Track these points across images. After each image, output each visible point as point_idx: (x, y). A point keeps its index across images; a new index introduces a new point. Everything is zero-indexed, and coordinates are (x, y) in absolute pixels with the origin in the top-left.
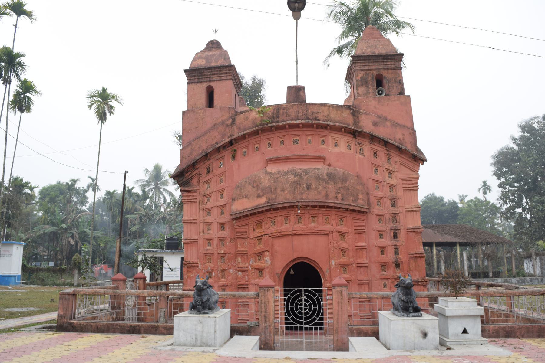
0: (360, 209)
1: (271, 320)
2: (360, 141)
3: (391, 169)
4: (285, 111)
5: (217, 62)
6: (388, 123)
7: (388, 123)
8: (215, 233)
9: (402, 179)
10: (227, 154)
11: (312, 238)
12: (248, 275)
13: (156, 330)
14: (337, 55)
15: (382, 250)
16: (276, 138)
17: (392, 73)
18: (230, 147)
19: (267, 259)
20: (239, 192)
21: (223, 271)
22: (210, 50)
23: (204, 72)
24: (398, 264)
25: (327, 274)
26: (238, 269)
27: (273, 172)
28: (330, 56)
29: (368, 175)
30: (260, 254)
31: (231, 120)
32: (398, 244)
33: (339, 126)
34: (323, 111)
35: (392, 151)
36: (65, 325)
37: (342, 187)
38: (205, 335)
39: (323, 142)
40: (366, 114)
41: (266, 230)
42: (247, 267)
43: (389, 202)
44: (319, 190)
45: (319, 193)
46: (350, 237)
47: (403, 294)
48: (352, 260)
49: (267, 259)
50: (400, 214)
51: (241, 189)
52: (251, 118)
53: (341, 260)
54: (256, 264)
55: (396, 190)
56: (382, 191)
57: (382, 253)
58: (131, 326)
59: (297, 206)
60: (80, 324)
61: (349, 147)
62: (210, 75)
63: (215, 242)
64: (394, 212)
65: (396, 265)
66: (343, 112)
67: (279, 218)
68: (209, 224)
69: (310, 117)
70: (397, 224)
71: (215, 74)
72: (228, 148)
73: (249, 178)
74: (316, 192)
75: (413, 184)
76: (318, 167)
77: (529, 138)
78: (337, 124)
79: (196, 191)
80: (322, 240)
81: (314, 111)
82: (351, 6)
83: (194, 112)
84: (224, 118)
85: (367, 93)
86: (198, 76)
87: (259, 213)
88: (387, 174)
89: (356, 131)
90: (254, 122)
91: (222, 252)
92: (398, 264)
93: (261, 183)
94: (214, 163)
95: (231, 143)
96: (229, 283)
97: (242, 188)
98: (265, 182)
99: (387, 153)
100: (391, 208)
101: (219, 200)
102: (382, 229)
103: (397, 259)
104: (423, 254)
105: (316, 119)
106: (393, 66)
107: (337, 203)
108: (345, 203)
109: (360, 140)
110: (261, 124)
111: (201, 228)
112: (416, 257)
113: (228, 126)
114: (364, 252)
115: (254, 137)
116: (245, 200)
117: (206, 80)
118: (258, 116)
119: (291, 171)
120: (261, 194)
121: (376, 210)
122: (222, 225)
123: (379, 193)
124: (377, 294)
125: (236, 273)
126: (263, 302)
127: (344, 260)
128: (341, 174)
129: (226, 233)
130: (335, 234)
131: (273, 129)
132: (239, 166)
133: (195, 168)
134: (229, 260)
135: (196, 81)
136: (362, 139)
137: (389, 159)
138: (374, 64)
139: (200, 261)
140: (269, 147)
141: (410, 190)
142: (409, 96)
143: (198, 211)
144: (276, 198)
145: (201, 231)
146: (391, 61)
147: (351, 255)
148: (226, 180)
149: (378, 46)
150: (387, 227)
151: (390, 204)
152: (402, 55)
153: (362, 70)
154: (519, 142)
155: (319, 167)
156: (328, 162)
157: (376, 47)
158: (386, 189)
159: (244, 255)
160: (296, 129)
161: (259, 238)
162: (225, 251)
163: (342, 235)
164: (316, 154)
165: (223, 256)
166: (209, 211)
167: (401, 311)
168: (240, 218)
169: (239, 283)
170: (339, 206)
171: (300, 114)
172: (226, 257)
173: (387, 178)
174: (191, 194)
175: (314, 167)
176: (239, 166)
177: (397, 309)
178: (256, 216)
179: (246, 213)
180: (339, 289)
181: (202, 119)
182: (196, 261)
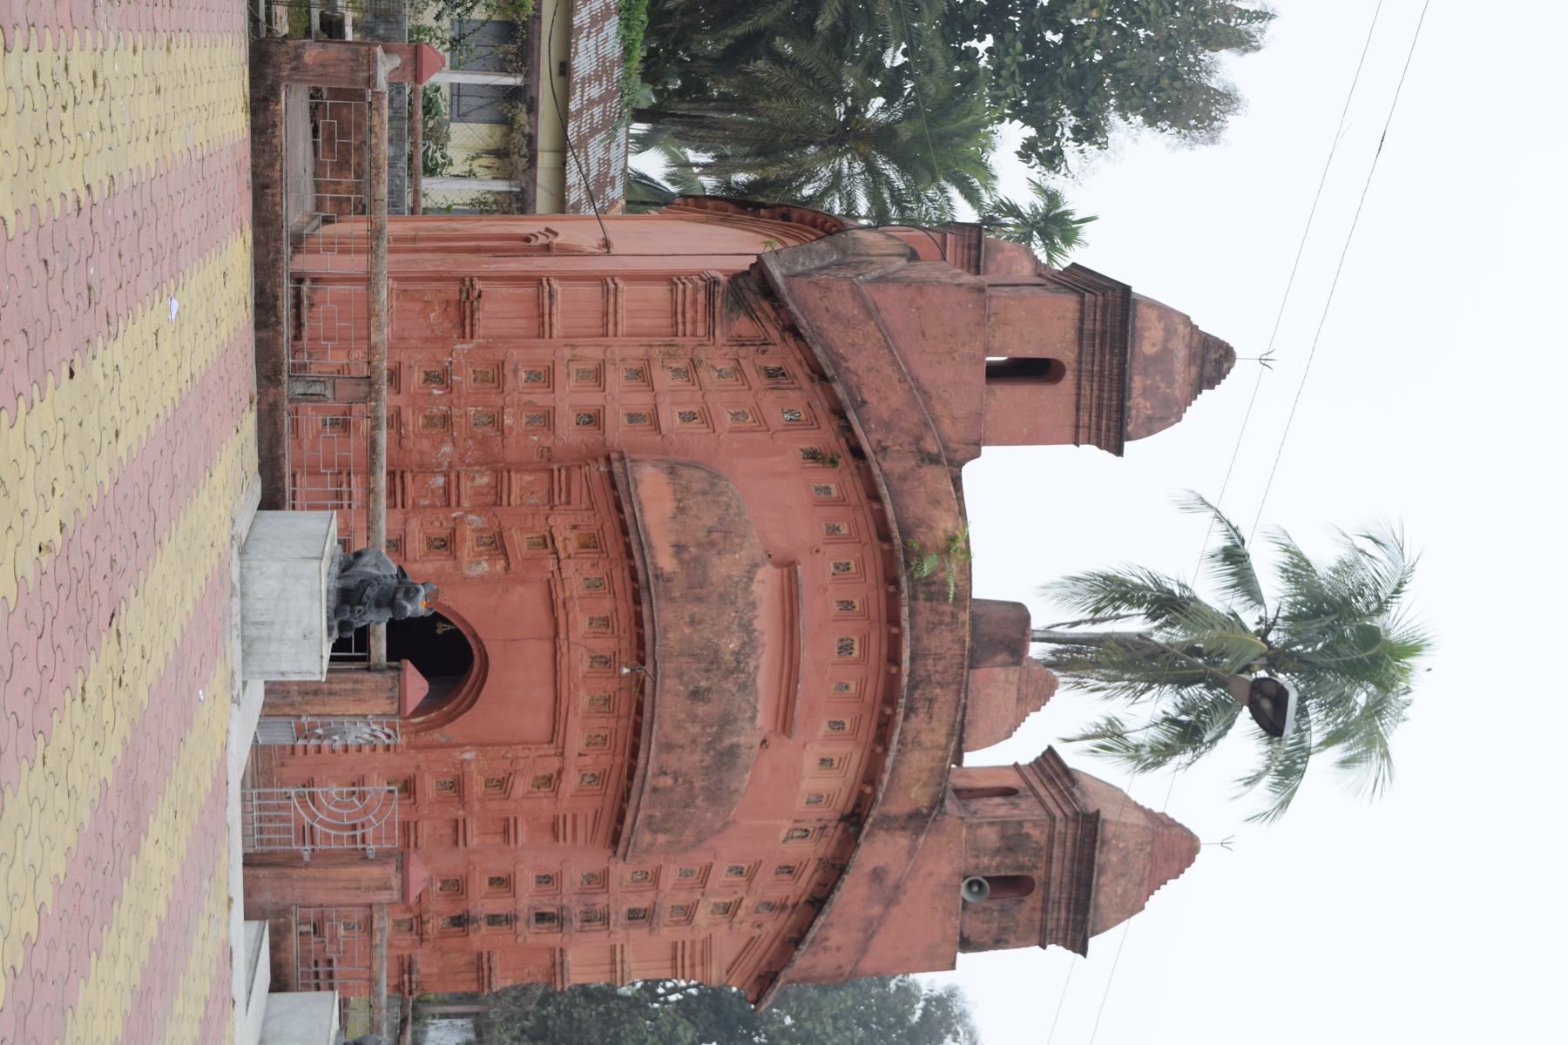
0: (624, 836)
1: (309, 708)
2: (830, 830)
3: (741, 913)
4: (947, 619)
5: (1143, 395)
6: (877, 910)
7: (877, 910)
8: (569, 398)
9: (708, 943)
10: (825, 436)
11: (543, 694)
12: (433, 506)
13: (268, 378)
14: (1220, 541)
15: (502, 883)
16: (865, 591)
17: (1031, 920)
18: (845, 448)
19: (485, 566)
20: (696, 487)
21: (446, 420)
23: (1112, 354)
24: (461, 922)
26: (453, 476)
27: (754, 587)
28: (1220, 518)
30: (497, 545)
31: (935, 450)
32: (520, 925)
33: (881, 781)
35: (794, 916)
36: (269, 71)
37: (692, 788)
38: (273, 648)
39: (837, 725)
40: (911, 852)
41: (572, 562)
42: (458, 504)
44: (688, 725)
46: (544, 805)
48: (476, 806)
49: (485, 566)
51: (704, 493)
52: (937, 513)
53: (476, 775)
55: (677, 923)
56: (676, 887)
57: (492, 881)
58: (276, 298)
60: (274, 125)
61: (817, 800)
62: (1102, 376)
63: (540, 398)
64: (613, 917)
66: (925, 785)
68: (598, 376)
69: (917, 694)
70: (577, 924)
71: (1101, 390)
72: (842, 441)
73: (740, 514)
74: (683, 716)
75: (693, 966)
77: (902, 1019)
78: (886, 778)
79: (710, 332)
80: (536, 724)
81: (936, 706)
83: (979, 324)
84: (946, 426)
85: (977, 851)
86: (1104, 333)
87: (628, 547)
88: (727, 900)
89: (860, 826)
90: (920, 523)
91: (508, 421)
94: (799, 397)
95: (857, 452)
97: (710, 498)
98: (722, 568)
99: (790, 903)
100: (624, 909)
101: (677, 410)
102: (566, 885)
103: (476, 920)
104: (490, 987)
105: (911, 710)
106: (1051, 925)
108: (645, 798)
109: (834, 833)
112: (479, 968)
113: (918, 439)
114: (499, 839)
115: (871, 522)
116: (669, 507)
117: (1086, 358)
119: (752, 640)
120: (686, 556)
121: (621, 872)
122: (593, 419)
123: (670, 876)
125: (440, 465)
126: (358, 686)
127: (476, 787)
128: (734, 785)
129: (568, 432)
131: (892, 589)
132: (784, 475)
133: (786, 335)
134: (483, 442)
135: (1088, 325)
137: (771, 907)
138: (1067, 874)
139: (479, 346)
140: (837, 567)
141: (674, 958)
143: (645, 340)
144: (672, 599)
145: (578, 351)
146: (1067, 920)
149: (1123, 882)
151: (636, 906)
153: (1051, 838)
155: (759, 721)
156: (773, 740)
157: (1123, 875)
158: (683, 898)
159: (496, 498)
160: (884, 651)
162: (511, 428)
163: (551, 782)
165: (496, 421)
166: (641, 375)
168: (614, 486)
169: (408, 477)
170: (637, 780)
171: (930, 662)
172: (489, 431)
173: (713, 900)
174: (700, 316)
175: (760, 706)
176: (784, 475)
178: (619, 534)
179: (627, 509)
180: (395, 882)
182: (479, 331)
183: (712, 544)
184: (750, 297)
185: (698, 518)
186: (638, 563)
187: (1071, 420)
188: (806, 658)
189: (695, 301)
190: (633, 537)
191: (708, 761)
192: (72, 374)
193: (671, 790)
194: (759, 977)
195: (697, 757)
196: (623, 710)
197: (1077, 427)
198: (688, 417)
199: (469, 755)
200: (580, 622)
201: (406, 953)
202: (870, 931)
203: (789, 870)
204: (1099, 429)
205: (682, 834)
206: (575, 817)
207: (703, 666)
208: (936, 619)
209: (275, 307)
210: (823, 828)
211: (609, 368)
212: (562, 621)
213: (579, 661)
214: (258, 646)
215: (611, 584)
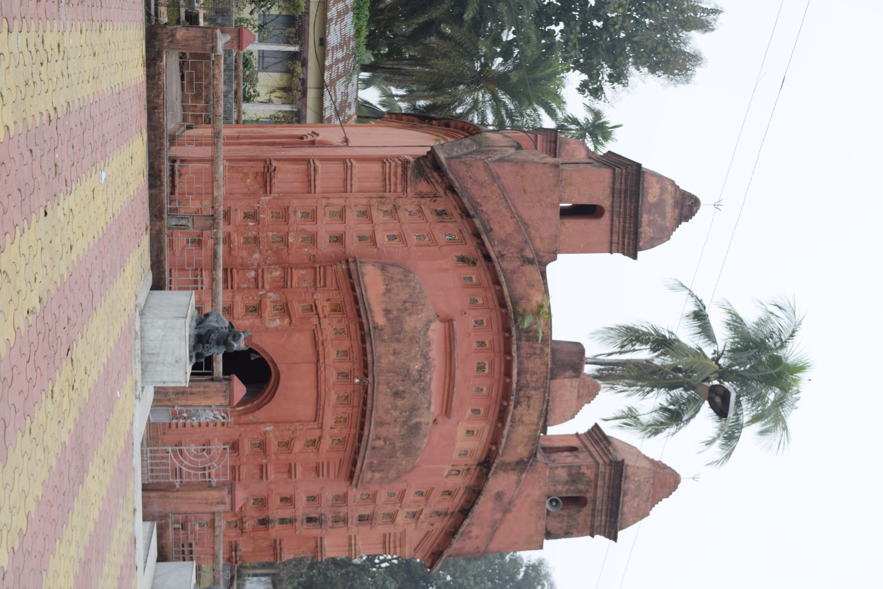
0: (356, 474)
1: (179, 402)
2: (472, 471)
3: (422, 517)
4: (538, 352)
5: (648, 225)
6: (498, 516)
7: (498, 516)
8: (325, 227)
9: (403, 534)
10: (469, 249)
11: (311, 394)
12: (249, 288)
13: (156, 216)
15: (288, 500)
16: (491, 336)
17: (585, 522)
18: (480, 255)
19: (278, 322)
20: (397, 277)
21: (256, 239)
23: (631, 202)
24: (264, 522)
25: (251, 417)
26: (260, 271)
27: (429, 333)
29: (414, 483)
30: (285, 310)
31: (530, 256)
32: (298, 524)
33: (501, 443)
34: (530, 414)
35: (452, 520)
36: (157, 43)
37: (394, 447)
38: (159, 368)
39: (476, 411)
40: (518, 483)
42: (263, 287)
43: (366, 511)
44: (392, 411)
46: (312, 457)
48: (273, 457)
49: (278, 322)
51: (401, 281)
52: (532, 292)
54: (268, 303)
55: (386, 523)
56: (386, 503)
57: (282, 499)
58: (160, 171)
59: (367, 376)
60: (160, 74)
61: (465, 453)
62: (625, 214)
63: (309, 227)
64: (350, 520)
65: (264, 520)
68: (341, 215)
69: (521, 394)
70: (330, 523)
71: (625, 222)
72: (479, 251)
73: (421, 293)
74: (389, 406)
75: (395, 547)
77: (513, 577)
78: (504, 441)
79: (405, 190)
80: (308, 411)
81: (532, 401)
82: (789, 346)
84: (538, 243)
85: (555, 482)
86: (626, 190)
87: (358, 311)
88: (414, 510)
91: (291, 240)
93: (410, 314)
94: (455, 226)
95: (487, 257)
96: (235, 253)
98: (411, 323)
99: (449, 512)
100: (356, 515)
102: (323, 501)
103: (272, 521)
105: (518, 403)
106: (597, 524)
108: (368, 453)
109: (474, 472)
110: (516, 314)
111: (335, 201)
112: (275, 548)
113: (522, 250)
115: (495, 297)
116: (382, 288)
117: (616, 205)
119: (428, 364)
120: (391, 316)
121: (355, 494)
122: (339, 239)
123: (382, 497)
124: (219, 549)
126: (206, 389)
127: (273, 446)
129: (325, 246)
130: (317, 433)
133: (447, 191)
134: (277, 252)
135: (617, 186)
137: (439, 514)
138: (606, 495)
139: (275, 198)
140: (476, 322)
141: (384, 543)
143: (367, 194)
144: (383, 341)
145: (330, 201)
146: (606, 521)
147: (282, 457)
148: (421, 246)
149: (637, 499)
150: (326, 510)
151: (363, 513)
152: (613, 536)
153: (597, 475)
155: (433, 409)
156: (440, 420)
157: (637, 496)
158: (389, 509)
159: (284, 283)
160: (503, 369)
162: (292, 244)
163: (315, 443)
165: (284, 240)
166: (366, 214)
168: (350, 277)
169: (235, 271)
170: (364, 442)
171: (529, 376)
172: (281, 246)
173: (406, 510)
174: (399, 181)
175: (433, 401)
179: (358, 290)
180: (228, 500)
181: (540, 201)
182: (275, 189)
184: (427, 170)
185: (398, 295)
188: (458, 374)
189: (396, 173)
190: (361, 305)
191: (403, 432)
192: (46, 214)
193: (383, 448)
194: (432, 553)
195: (397, 429)
196: (356, 403)
197: (611, 243)
198: (392, 238)
199: (269, 428)
201: (234, 540)
202: (495, 527)
203: (449, 493)
204: (623, 244)
205: (388, 473)
206: (328, 463)
207: (400, 378)
208: (532, 351)
209: (160, 176)
210: (468, 470)
211: (347, 209)
213: (331, 375)
214: (150, 366)
215: (349, 332)
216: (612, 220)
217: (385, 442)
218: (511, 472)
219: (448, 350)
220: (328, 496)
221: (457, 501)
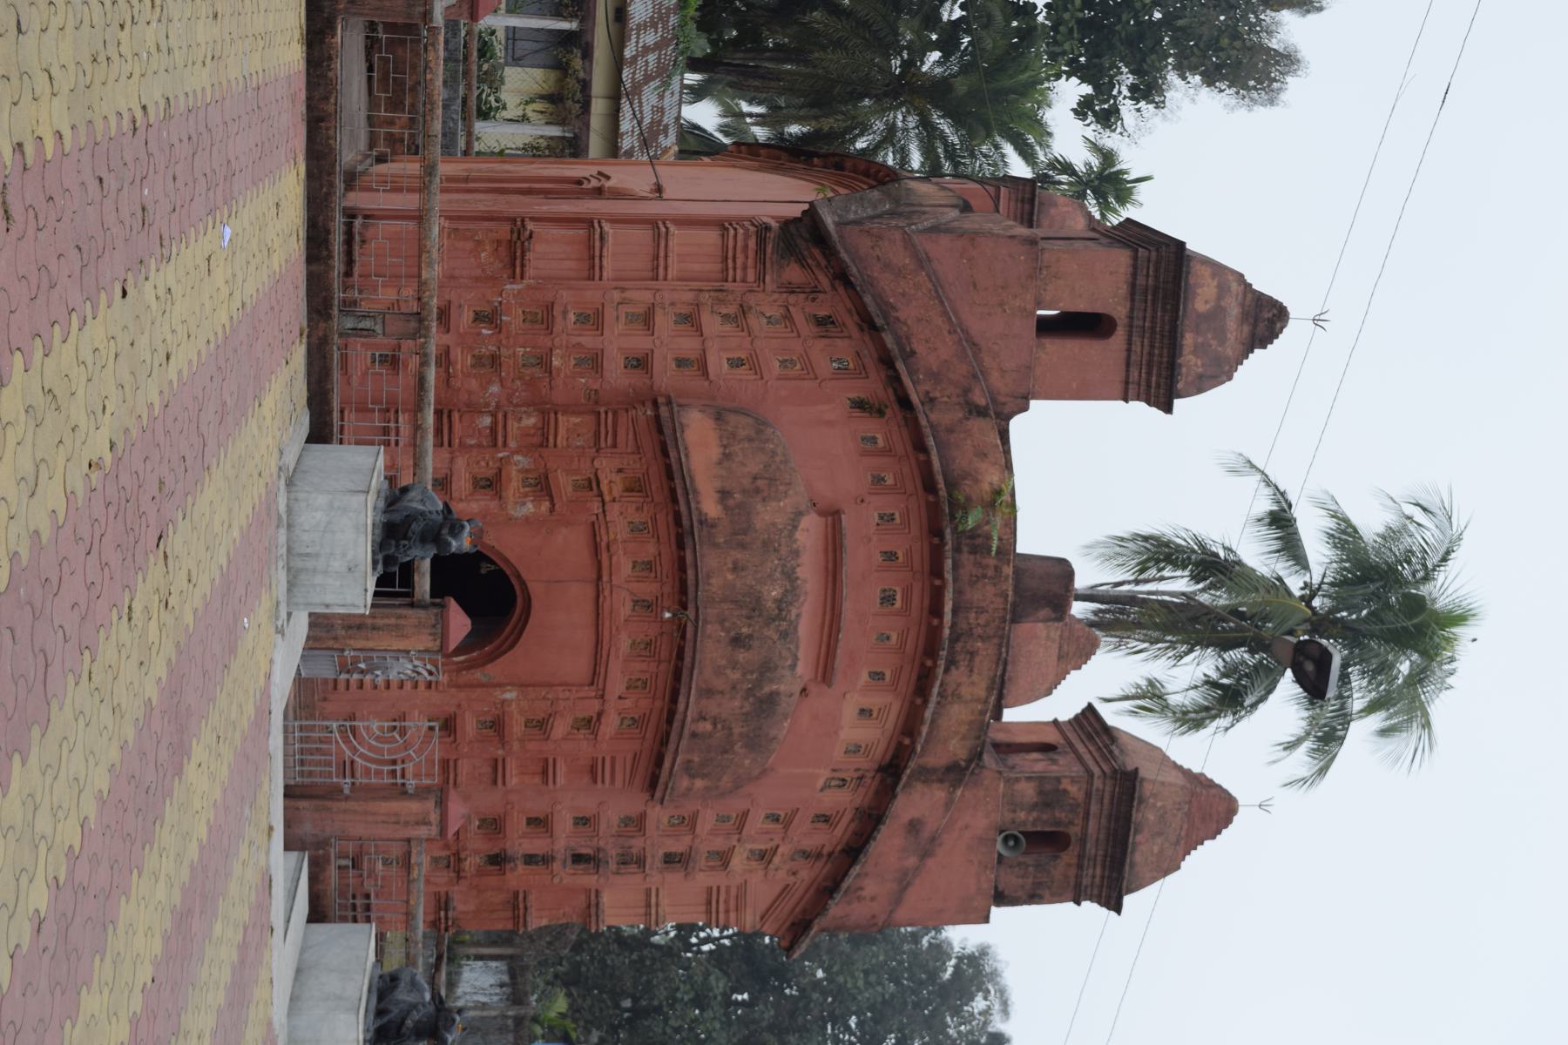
0: (662, 780)
2: (868, 781)
3: (776, 860)
4: (990, 573)
5: (1194, 353)
6: (912, 861)
7: (912, 861)
8: (618, 341)
9: (743, 888)
10: (873, 386)
11: (585, 637)
12: (480, 446)
13: (318, 312)
15: (540, 823)
18: (892, 398)
19: (530, 507)
21: (495, 360)
22: (1245, 316)
23: (1164, 310)
27: (798, 535)
28: (1268, 482)
30: (542, 486)
31: (982, 402)
32: (557, 866)
33: (920, 733)
34: (973, 683)
37: (731, 734)
38: (318, 580)
39: (877, 676)
40: (948, 804)
41: (617, 506)
42: (505, 444)
43: (677, 846)
45: (719, 672)
47: (419, 1021)
48: (516, 746)
49: (530, 507)
50: (641, 876)
51: (750, 440)
52: (983, 466)
54: (514, 473)
55: (712, 868)
58: (328, 232)
60: (330, 58)
61: (855, 749)
63: (589, 340)
64: (649, 861)
65: (497, 856)
66: (964, 738)
67: (651, 550)
68: (647, 319)
69: (958, 646)
70: (613, 866)
71: (1152, 346)
72: (890, 391)
73: (786, 462)
74: (724, 662)
76: (800, 665)
77: (933, 975)
78: (925, 730)
79: (761, 279)
80: (577, 665)
81: (977, 659)
82: (1440, 577)
85: (1013, 804)
86: (1156, 289)
87: (673, 491)
88: (763, 847)
89: (898, 777)
91: (556, 363)
92: (498, 861)
93: (764, 500)
95: (905, 403)
98: (767, 515)
99: (825, 851)
100: (661, 852)
102: (603, 826)
103: (512, 859)
104: (525, 925)
105: (951, 663)
106: (1086, 881)
107: (683, 722)
109: (871, 784)
110: (953, 504)
112: (515, 907)
113: (967, 391)
116: (715, 452)
117: (1138, 314)
118: (986, 487)
119: (794, 588)
120: (731, 502)
121: (658, 816)
122: (641, 363)
126: (402, 622)
127: (517, 727)
128: (773, 733)
129: (616, 375)
132: (830, 424)
133: (837, 283)
135: (1141, 281)
136: (873, 788)
137: (806, 855)
138: (1103, 831)
139: (529, 287)
140: (881, 517)
141: (709, 903)
142: (986, 920)
143: (695, 285)
144: (716, 545)
146: (1103, 877)
147: (531, 746)
148: (787, 379)
149: (1159, 840)
150: (607, 841)
153: (1088, 795)
154: (925, 941)
155: (800, 669)
156: (813, 689)
157: (1160, 834)
158: (719, 843)
159: (542, 440)
160: (926, 603)
161: (592, 484)
162: (559, 370)
163: (590, 724)
164: (840, 662)
165: (544, 362)
166: (690, 320)
167: (379, 1023)
168: (660, 431)
169: (456, 416)
170: (676, 725)
171: (972, 615)
172: (538, 372)
174: (750, 262)
175: (800, 655)
176: (830, 424)
177: (380, 1013)
180: (434, 817)
181: (1001, 304)
182: (530, 271)
183: (757, 491)
185: (743, 464)
186: (683, 508)
187: (1120, 376)
189: (746, 247)
190: (678, 481)
193: (710, 735)
194: (793, 924)
195: (737, 704)
196: (664, 654)
197: (1127, 383)
198: (736, 363)
200: (624, 567)
201: (443, 890)
203: (826, 819)
206: (613, 760)
207: (744, 612)
210: (861, 778)
212: (605, 563)
213: (621, 605)
214: (302, 577)
216: (1129, 342)
217: (715, 725)
218: (935, 785)
219: (830, 566)
220: (611, 816)
221: (840, 833)
